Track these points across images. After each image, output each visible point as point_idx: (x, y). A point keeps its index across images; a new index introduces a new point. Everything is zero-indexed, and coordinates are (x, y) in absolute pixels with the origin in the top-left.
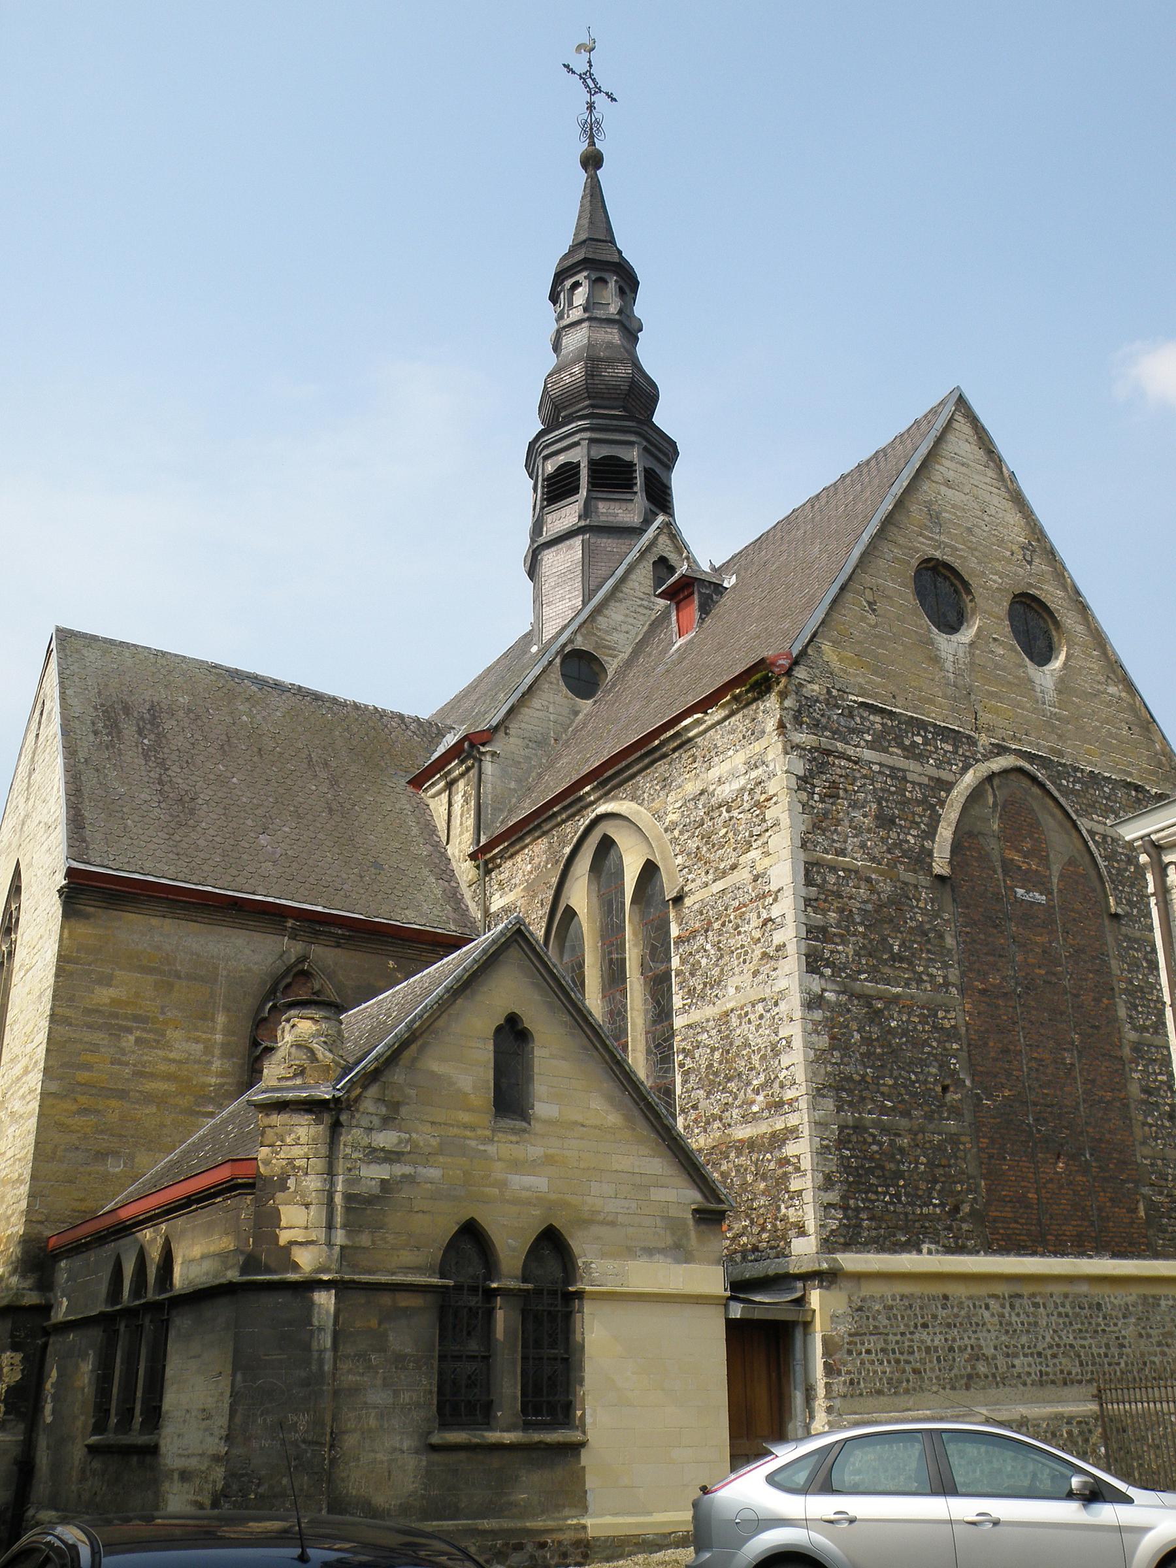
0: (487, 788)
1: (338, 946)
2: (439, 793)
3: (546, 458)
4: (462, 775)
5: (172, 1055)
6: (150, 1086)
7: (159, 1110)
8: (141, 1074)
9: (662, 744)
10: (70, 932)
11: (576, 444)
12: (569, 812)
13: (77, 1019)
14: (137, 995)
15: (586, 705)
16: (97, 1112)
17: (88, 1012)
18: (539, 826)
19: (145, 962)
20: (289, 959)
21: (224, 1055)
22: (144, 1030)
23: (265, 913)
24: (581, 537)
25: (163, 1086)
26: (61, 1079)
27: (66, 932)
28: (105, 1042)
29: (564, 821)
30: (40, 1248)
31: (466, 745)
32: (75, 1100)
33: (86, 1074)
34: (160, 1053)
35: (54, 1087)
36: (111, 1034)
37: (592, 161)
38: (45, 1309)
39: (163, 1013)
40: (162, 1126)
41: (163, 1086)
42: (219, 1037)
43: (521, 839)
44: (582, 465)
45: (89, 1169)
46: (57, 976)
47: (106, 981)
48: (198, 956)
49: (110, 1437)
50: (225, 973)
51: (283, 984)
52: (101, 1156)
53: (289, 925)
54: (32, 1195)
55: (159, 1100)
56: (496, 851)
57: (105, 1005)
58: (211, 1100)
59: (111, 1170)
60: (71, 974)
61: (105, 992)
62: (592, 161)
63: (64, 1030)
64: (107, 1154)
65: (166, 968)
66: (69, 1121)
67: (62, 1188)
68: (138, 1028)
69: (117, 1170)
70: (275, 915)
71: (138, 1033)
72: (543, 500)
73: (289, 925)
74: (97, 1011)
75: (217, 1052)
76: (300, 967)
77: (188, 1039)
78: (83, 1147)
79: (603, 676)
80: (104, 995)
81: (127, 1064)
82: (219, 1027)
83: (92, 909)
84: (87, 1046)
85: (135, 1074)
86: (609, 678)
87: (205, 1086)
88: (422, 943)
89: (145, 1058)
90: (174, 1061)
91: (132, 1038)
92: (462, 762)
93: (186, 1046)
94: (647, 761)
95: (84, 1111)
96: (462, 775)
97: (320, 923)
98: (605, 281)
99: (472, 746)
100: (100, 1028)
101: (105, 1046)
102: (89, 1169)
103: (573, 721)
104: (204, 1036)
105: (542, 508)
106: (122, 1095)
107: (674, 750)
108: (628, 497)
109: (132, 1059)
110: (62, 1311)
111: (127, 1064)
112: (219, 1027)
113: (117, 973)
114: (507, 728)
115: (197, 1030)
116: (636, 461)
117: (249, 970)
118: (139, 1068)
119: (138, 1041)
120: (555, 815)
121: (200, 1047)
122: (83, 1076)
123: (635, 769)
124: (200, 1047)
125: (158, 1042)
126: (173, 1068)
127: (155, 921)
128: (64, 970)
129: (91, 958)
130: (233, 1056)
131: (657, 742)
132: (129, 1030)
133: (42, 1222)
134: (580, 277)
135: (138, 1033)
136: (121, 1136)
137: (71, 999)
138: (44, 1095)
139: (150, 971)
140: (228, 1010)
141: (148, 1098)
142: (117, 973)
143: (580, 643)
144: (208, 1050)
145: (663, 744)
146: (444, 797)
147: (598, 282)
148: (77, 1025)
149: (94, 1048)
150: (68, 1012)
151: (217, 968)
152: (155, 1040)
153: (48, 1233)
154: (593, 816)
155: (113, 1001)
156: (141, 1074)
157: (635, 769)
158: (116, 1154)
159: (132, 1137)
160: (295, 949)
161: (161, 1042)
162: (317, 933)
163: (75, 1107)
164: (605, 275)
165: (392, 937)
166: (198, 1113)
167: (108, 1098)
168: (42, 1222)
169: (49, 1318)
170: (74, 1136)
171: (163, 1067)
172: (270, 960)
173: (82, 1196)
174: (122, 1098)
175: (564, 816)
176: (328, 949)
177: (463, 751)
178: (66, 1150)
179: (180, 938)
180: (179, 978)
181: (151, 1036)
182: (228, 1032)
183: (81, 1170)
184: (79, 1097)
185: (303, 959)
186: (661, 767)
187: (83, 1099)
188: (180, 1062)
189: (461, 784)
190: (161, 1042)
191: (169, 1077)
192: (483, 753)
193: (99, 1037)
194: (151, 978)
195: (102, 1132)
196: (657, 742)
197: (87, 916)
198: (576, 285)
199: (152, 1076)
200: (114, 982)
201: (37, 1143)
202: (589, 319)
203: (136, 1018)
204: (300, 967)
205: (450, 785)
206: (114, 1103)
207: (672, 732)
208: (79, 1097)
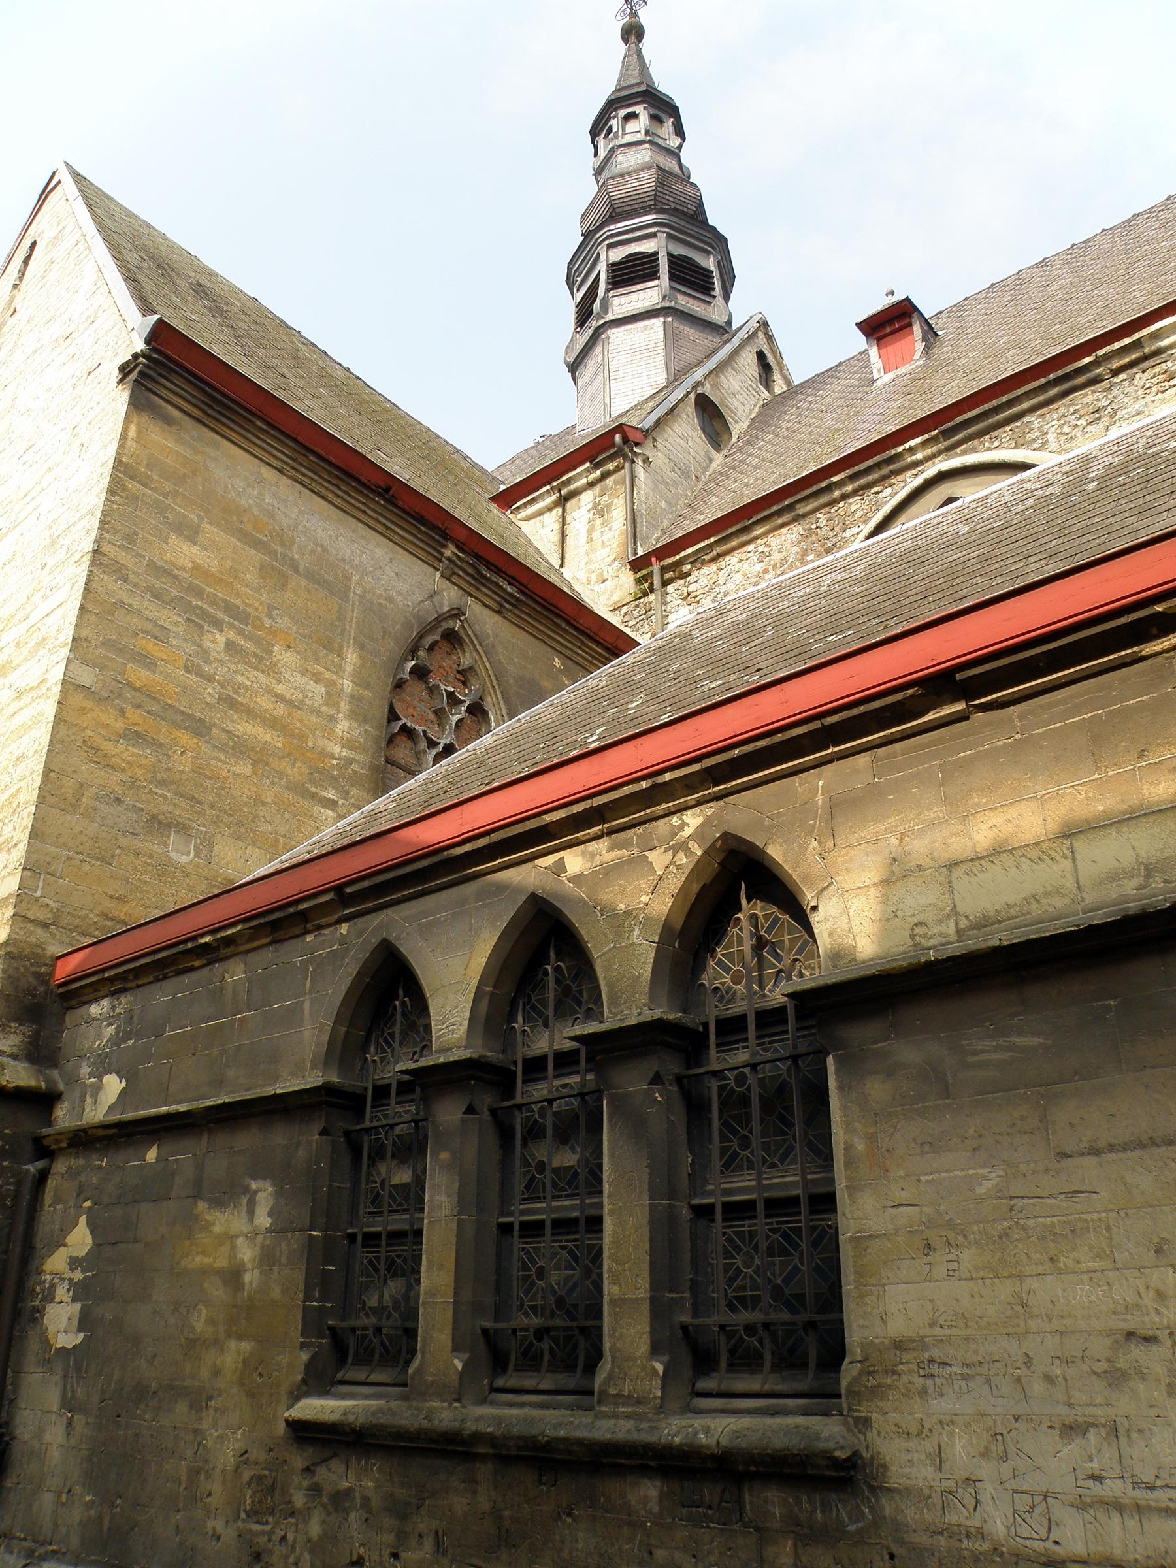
0: (640, 494)
1: (498, 612)
2: (550, 509)
3: (610, 246)
4: (591, 485)
5: (280, 688)
6: (245, 728)
7: (255, 772)
8: (232, 704)
9: (1097, 363)
10: (139, 432)
11: (654, 235)
12: (857, 484)
13: (137, 574)
14: (233, 572)
15: (718, 458)
16: (157, 745)
17: (154, 568)
18: (791, 507)
19: (248, 527)
20: (441, 605)
21: (353, 715)
22: (240, 632)
23: (422, 520)
24: (662, 319)
25: (264, 735)
26: (102, 667)
27: (132, 431)
28: (180, 630)
29: (844, 497)
30: (37, 975)
31: (618, 438)
32: (122, 711)
33: (145, 673)
34: (262, 677)
35: (87, 676)
36: (188, 620)
37: (633, 33)
38: (42, 1101)
39: (270, 617)
40: (259, 801)
41: (264, 735)
42: (347, 684)
43: (746, 529)
44: (660, 255)
45: (137, 844)
46: (111, 491)
47: (191, 534)
48: (325, 550)
49: (441, 1386)
50: (359, 591)
51: (429, 640)
52: (159, 825)
53: (448, 553)
54: (30, 867)
55: (258, 756)
56: (690, 550)
57: (183, 568)
58: (334, 781)
59: (173, 855)
60: (135, 498)
61: (185, 547)
62: (633, 33)
63: (110, 584)
64: (169, 826)
65: (279, 549)
66: (108, 747)
67: (87, 867)
68: (231, 626)
69: (185, 859)
70: (434, 527)
71: (231, 635)
72: (608, 283)
73: (448, 553)
74: (169, 573)
75: (344, 706)
76: (450, 624)
77: (304, 672)
78: (128, 800)
79: (725, 437)
80: (184, 553)
81: (211, 679)
82: (349, 669)
83: (176, 413)
84: (149, 626)
85: (224, 700)
86: (734, 439)
87: (325, 754)
88: (598, 643)
89: (240, 678)
90: (281, 698)
91: (221, 639)
92: (597, 466)
93: (301, 681)
94: (1053, 392)
95: (136, 737)
96: (591, 485)
97: (489, 565)
98: (661, 122)
99: (625, 440)
100: (172, 603)
101: (177, 636)
102: (137, 844)
103: (708, 467)
104: (327, 675)
105: (608, 291)
106: (200, 728)
107: (1116, 373)
108: (707, 299)
109: (220, 672)
110: (105, 1097)
111: (211, 679)
112: (349, 669)
113: (205, 526)
114: (654, 440)
115: (317, 660)
116: (712, 268)
117: (390, 599)
118: (229, 691)
119: (230, 646)
120: (829, 488)
121: (321, 689)
122: (139, 675)
123: (1026, 405)
124: (321, 689)
125: (261, 659)
126: (280, 710)
127: (267, 473)
128: (124, 489)
129: (168, 486)
130: (365, 721)
131: (1087, 360)
132: (218, 625)
133: (45, 925)
134: (638, 109)
135: (231, 635)
136: (193, 799)
137: (131, 538)
138: (69, 685)
139: (256, 544)
140: (362, 647)
141: (239, 748)
142: (205, 526)
143: (707, 389)
144: (332, 697)
145: (1097, 363)
146: (551, 519)
147: (655, 118)
148: (136, 585)
149: (160, 634)
150: (123, 557)
151: (350, 580)
152: (256, 655)
153: (55, 950)
154: (918, 481)
155: (196, 567)
156: (232, 704)
157: (1026, 405)
158: (183, 829)
159: (212, 806)
160: (450, 596)
161: (263, 662)
162: (480, 579)
163: (119, 725)
164: (663, 116)
165: (568, 622)
166: (313, 796)
167: (178, 727)
168: (45, 925)
169: (49, 1124)
170: (116, 777)
171: (265, 703)
172: (418, 597)
173: (122, 892)
174: (197, 734)
175: (849, 488)
176: (487, 612)
177: (613, 445)
178: (97, 798)
179: (301, 512)
180: (297, 571)
181: (250, 646)
182: (360, 681)
183: (123, 841)
184: (130, 712)
185: (457, 613)
186: (1089, 397)
187: (134, 714)
188: (290, 703)
189: (587, 497)
190: (263, 662)
191: (273, 723)
192: (635, 454)
193: (168, 617)
194: (256, 556)
195: (162, 783)
196: (1087, 360)
197: (168, 421)
198: (633, 116)
199: (249, 713)
200: (200, 538)
201: (48, 771)
202: (650, 142)
203: (229, 608)
204: (450, 624)
205: (563, 501)
206: (184, 738)
207: (1127, 341)
208: (130, 712)
